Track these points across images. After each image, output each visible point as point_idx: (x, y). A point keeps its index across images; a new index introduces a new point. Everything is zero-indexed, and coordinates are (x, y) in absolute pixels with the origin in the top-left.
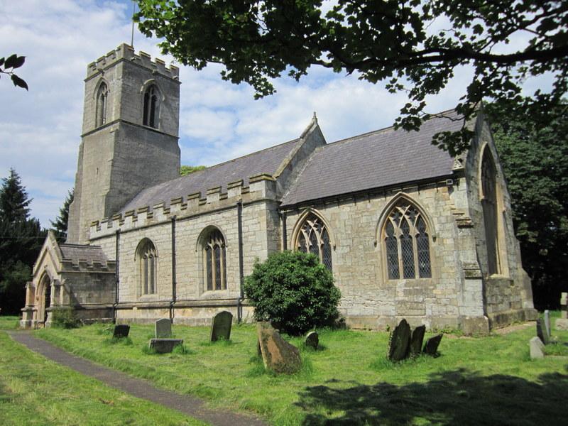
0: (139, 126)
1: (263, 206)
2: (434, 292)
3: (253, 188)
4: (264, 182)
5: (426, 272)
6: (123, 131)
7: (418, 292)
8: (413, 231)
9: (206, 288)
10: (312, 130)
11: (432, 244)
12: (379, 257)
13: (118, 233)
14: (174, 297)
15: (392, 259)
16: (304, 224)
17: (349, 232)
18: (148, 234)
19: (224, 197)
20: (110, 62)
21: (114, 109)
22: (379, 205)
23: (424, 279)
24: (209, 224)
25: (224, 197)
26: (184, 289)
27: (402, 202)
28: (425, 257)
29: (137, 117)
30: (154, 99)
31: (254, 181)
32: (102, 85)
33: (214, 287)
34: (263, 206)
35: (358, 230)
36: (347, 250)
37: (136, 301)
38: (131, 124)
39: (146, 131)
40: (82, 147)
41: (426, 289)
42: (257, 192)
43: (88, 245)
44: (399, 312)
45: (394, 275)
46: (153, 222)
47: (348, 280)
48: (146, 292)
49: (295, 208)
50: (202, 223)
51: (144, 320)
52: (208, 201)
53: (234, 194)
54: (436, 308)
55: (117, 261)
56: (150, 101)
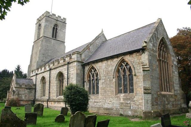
0: (50, 38)
4: (76, 54)
5: (132, 91)
6: (44, 40)
7: (129, 99)
8: (128, 73)
9: (59, 95)
10: (100, 35)
11: (134, 78)
12: (114, 84)
14: (35, 98)
15: (119, 85)
16: (91, 71)
17: (105, 74)
19: (64, 60)
20: (42, 17)
22: (116, 61)
23: (131, 94)
24: (60, 71)
25: (64, 60)
28: (132, 84)
29: (50, 34)
30: (57, 29)
32: (40, 25)
33: (61, 95)
34: (75, 64)
36: (104, 81)
37: (40, 98)
38: (47, 37)
39: (53, 40)
40: (33, 46)
43: (30, 79)
44: (121, 107)
46: (46, 70)
47: (104, 93)
48: (60, 95)
49: (88, 64)
52: (60, 62)
53: (67, 59)
54: (134, 106)
55: (36, 84)
56: (55, 30)
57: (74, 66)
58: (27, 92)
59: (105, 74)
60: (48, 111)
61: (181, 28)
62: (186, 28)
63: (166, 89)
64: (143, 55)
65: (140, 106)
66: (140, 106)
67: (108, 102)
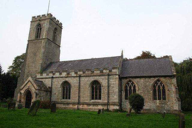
1: (117, 76)
2: (167, 104)
3: (113, 71)
5: (164, 99)
7: (162, 104)
13: (52, 78)
15: (154, 95)
17: (143, 86)
18: (67, 79)
21: (44, 34)
22: (152, 81)
24: (95, 79)
26: (83, 99)
27: (130, 81)
29: (51, 38)
31: (114, 68)
35: (145, 86)
37: (60, 101)
40: (28, 45)
41: (165, 103)
42: (115, 72)
45: (155, 99)
49: (126, 78)
50: (92, 79)
51: (65, 108)
55: (52, 87)
57: (116, 78)
58: (45, 95)
59: (143, 86)
60: (16, 113)
61: (145, 51)
62: (148, 52)
63: (96, 95)
64: (173, 79)
65: (171, 108)
66: (171, 108)
67: (146, 105)
